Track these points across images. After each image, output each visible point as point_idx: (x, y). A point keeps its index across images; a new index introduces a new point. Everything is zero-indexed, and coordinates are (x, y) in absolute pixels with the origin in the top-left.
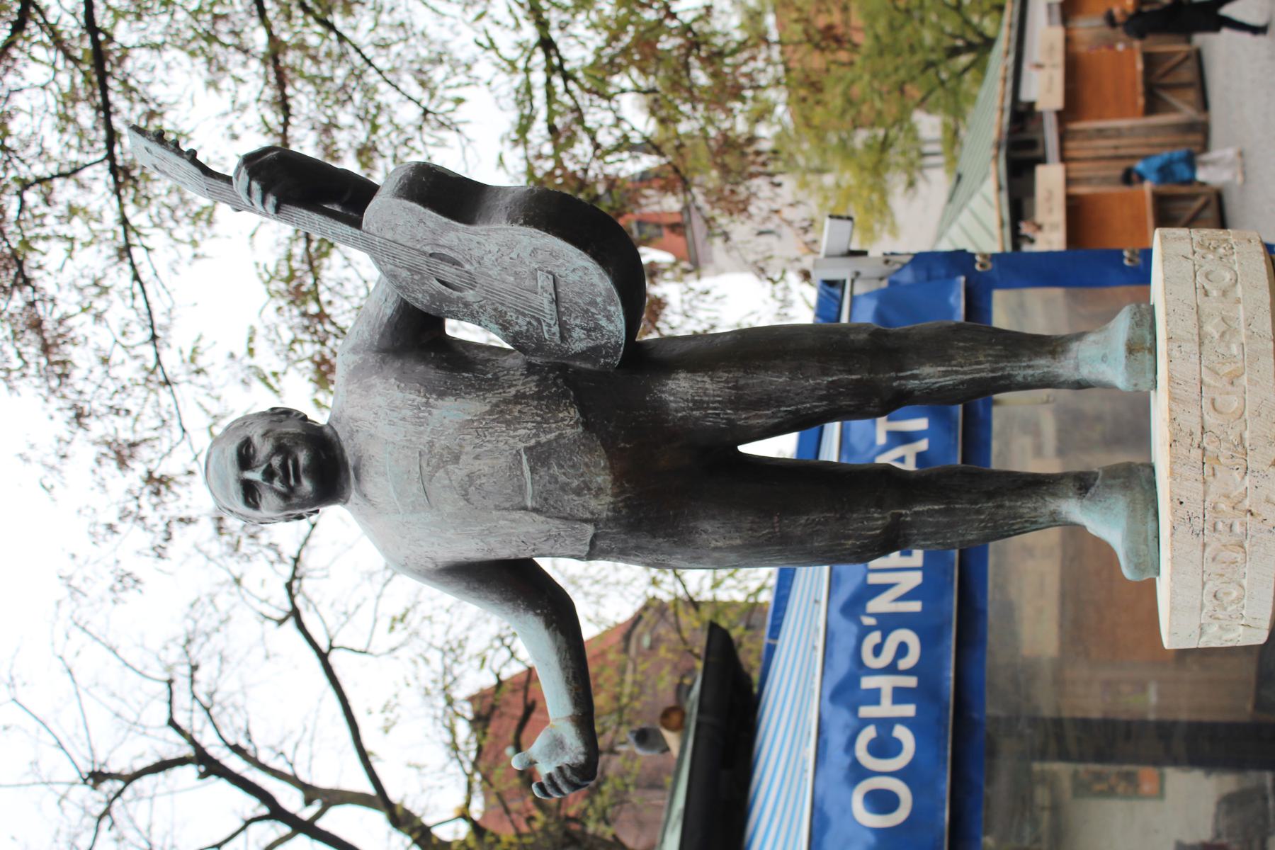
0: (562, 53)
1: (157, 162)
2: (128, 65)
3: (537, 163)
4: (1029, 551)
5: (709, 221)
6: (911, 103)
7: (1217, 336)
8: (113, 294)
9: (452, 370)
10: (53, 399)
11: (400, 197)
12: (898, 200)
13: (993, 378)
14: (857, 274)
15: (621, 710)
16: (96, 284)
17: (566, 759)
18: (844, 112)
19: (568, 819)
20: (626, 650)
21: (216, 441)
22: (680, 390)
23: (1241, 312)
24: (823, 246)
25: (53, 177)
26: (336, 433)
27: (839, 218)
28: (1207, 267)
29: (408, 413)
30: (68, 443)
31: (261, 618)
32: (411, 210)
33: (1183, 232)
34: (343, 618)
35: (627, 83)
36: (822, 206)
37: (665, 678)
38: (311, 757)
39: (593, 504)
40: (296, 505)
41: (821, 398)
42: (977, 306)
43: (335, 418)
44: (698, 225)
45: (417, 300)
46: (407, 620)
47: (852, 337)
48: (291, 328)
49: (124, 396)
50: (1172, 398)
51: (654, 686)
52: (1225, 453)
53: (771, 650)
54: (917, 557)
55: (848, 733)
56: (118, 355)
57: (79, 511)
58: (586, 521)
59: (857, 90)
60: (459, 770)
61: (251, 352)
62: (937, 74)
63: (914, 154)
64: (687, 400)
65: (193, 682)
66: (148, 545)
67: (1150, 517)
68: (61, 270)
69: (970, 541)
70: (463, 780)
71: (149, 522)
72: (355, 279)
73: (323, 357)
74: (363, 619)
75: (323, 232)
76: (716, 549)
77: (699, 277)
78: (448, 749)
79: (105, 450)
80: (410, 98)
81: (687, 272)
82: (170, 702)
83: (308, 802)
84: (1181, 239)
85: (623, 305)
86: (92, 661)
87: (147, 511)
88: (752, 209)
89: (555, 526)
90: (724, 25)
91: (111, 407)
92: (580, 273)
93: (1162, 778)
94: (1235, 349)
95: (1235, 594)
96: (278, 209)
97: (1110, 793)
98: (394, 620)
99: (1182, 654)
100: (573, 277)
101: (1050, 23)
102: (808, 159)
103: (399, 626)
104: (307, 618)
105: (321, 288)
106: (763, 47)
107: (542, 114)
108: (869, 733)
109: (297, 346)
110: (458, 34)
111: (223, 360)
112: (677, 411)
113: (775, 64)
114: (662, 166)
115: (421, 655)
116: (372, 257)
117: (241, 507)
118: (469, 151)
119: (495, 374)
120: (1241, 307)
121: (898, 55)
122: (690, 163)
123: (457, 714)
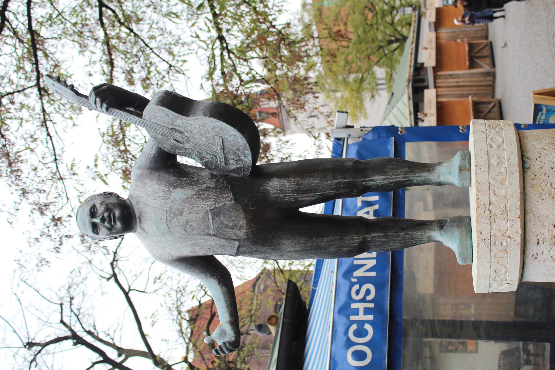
0: (227, 42)
1: (57, 89)
2: (46, 45)
3: (216, 88)
4: (422, 250)
5: (288, 112)
6: (373, 63)
7: (495, 164)
8: (39, 142)
9: (180, 177)
10: (13, 186)
11: (158, 105)
12: (367, 104)
13: (404, 181)
14: (350, 135)
15: (251, 316)
16: (31, 137)
17: (227, 339)
18: (345, 66)
19: (229, 362)
20: (253, 291)
21: (82, 205)
22: (274, 186)
23: (505, 154)
24: (335, 123)
25: (14, 92)
26: (131, 203)
27: (342, 112)
28: (491, 136)
29: (161, 195)
30: (19, 204)
31: (100, 278)
32: (163, 110)
33: (482, 121)
34: (135, 278)
35: (254, 55)
36: (336, 106)
37: (270, 303)
38: (121, 336)
39: (238, 233)
40: (113, 233)
41: (333, 189)
42: (399, 150)
43: (131, 196)
44: (284, 113)
45: (165, 147)
46: (161, 279)
47: (346, 164)
48: (113, 156)
49: (43, 184)
50: (477, 190)
51: (265, 306)
52: (499, 212)
53: (314, 291)
54: (374, 254)
55: (346, 326)
56: (40, 166)
57: (24, 233)
58: (235, 240)
59: (350, 58)
60: (184, 341)
61: (96, 165)
62: (384, 51)
63: (374, 84)
64: (278, 190)
65: (71, 304)
66: (53, 247)
67: (469, 239)
68: (17, 131)
69: (395, 248)
70: (185, 345)
71: (53, 237)
72: (140, 137)
73: (126, 168)
74: (143, 278)
75: (126, 119)
76: (289, 251)
77: (284, 135)
78: (179, 333)
79: (35, 207)
80: (164, 60)
81: (280, 133)
82: (62, 313)
83: (120, 355)
84: (481, 124)
85: (251, 150)
86: (29, 296)
87: (52, 232)
88: (306, 107)
89: (222, 242)
90: (295, 30)
91: (38, 189)
92: (233, 137)
93: (477, 345)
94: (503, 170)
95: (503, 271)
96: (107, 110)
97: (456, 350)
98: (156, 278)
99: (484, 295)
100: (230, 139)
101: (430, 31)
102: (330, 86)
103: (158, 281)
104: (119, 277)
105: (126, 139)
106: (312, 40)
107: (219, 67)
108: (354, 327)
109: (115, 164)
110: (185, 32)
111: (84, 168)
112: (273, 194)
113: (316, 47)
114: (269, 88)
115: (167, 293)
116: (147, 130)
117: (91, 233)
118: (188, 82)
119: (197, 179)
120: (505, 152)
121: (367, 43)
122: (281, 87)
123: (182, 318)
